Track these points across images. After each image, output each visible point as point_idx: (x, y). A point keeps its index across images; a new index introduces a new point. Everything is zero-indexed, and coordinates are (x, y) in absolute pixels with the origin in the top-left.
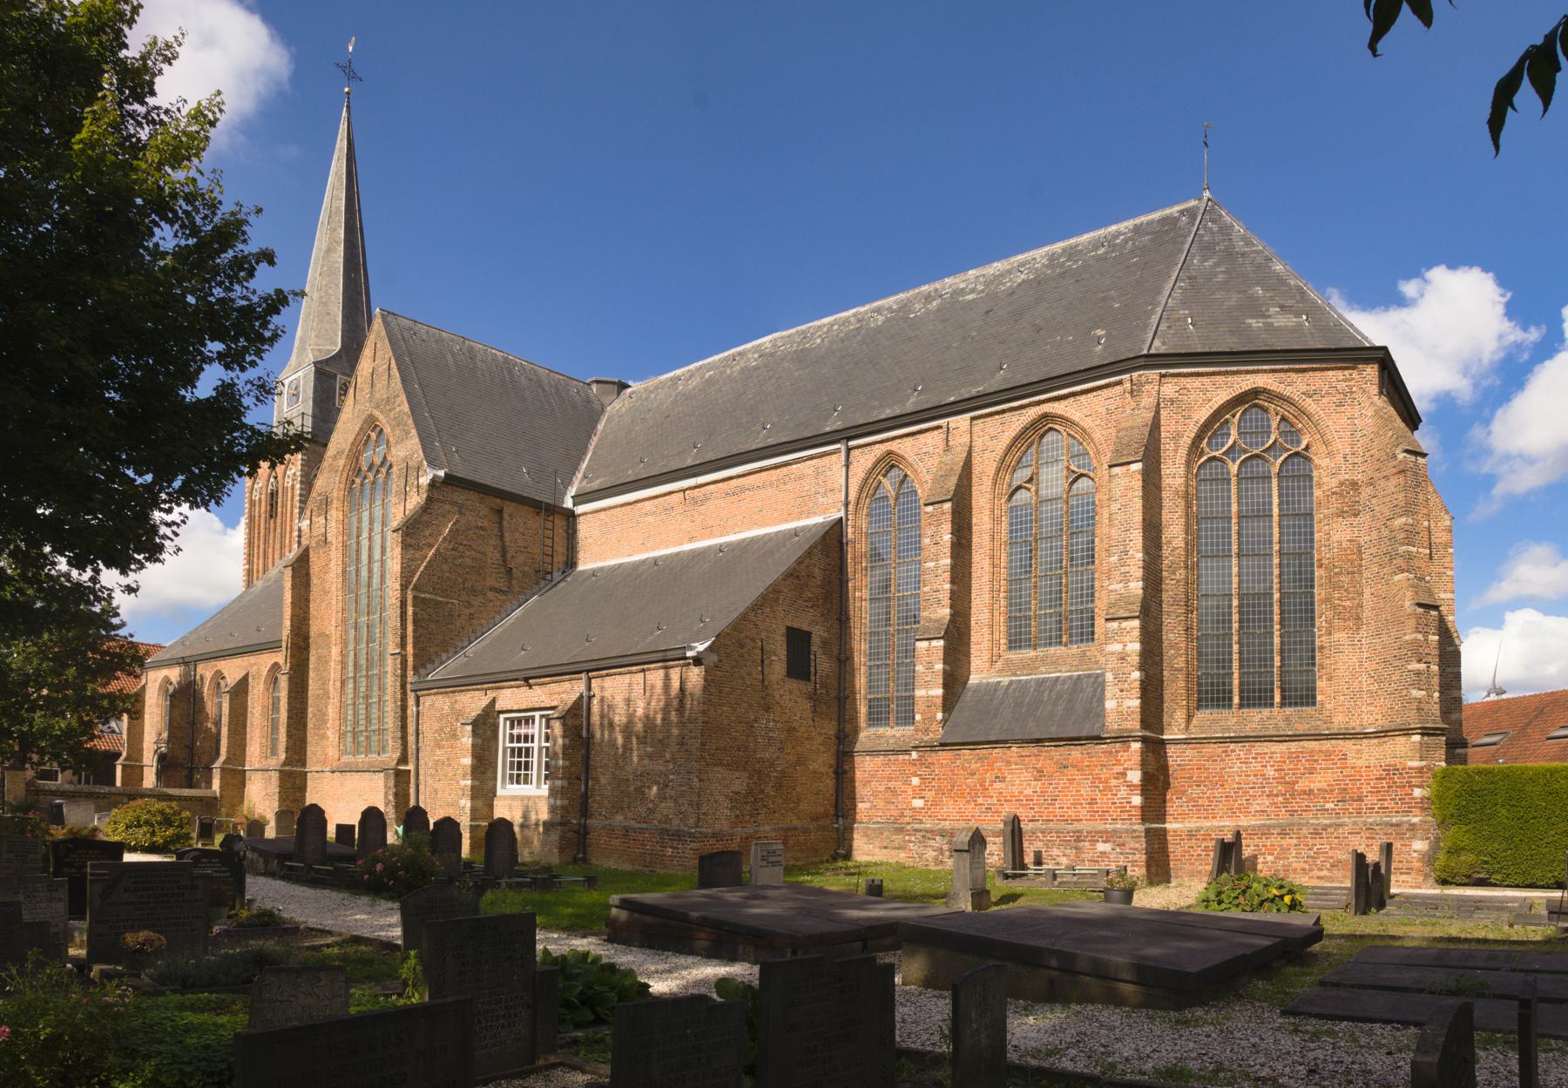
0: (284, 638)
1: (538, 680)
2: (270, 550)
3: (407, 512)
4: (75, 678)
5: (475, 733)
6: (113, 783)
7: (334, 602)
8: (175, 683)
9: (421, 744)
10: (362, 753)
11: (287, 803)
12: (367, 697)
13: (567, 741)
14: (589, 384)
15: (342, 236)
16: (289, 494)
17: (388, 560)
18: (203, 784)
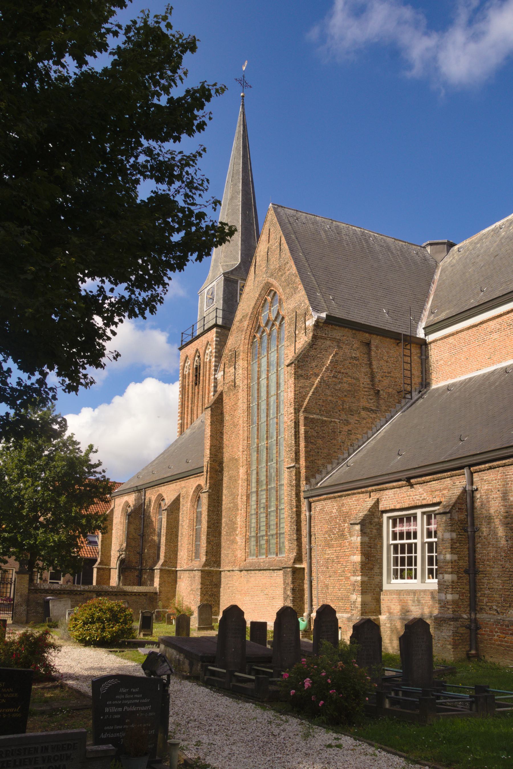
0: (205, 464)
1: (419, 479)
2: (195, 408)
3: (297, 351)
4: (65, 503)
5: (363, 532)
6: (92, 583)
7: (241, 432)
8: (132, 506)
9: (313, 545)
10: (263, 554)
11: (207, 597)
12: (267, 507)
13: (454, 535)
14: (424, 247)
15: (241, 187)
16: (208, 367)
17: (282, 394)
18: (149, 582)
